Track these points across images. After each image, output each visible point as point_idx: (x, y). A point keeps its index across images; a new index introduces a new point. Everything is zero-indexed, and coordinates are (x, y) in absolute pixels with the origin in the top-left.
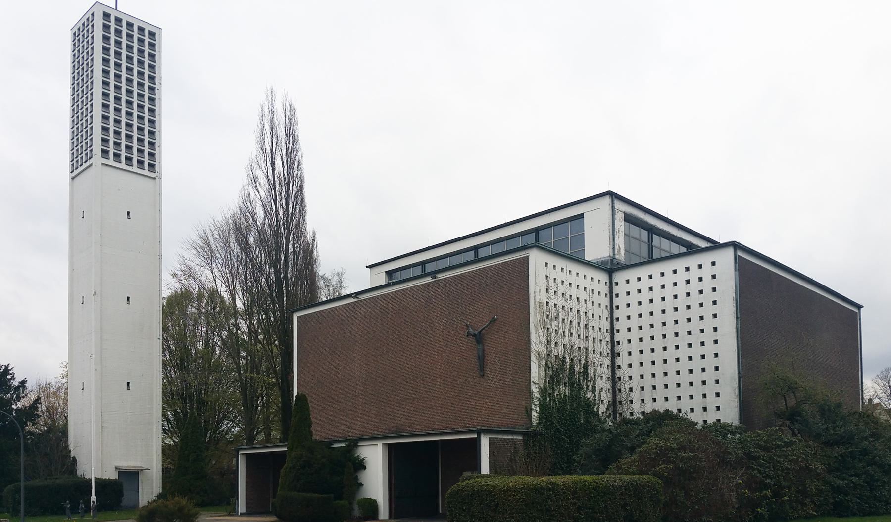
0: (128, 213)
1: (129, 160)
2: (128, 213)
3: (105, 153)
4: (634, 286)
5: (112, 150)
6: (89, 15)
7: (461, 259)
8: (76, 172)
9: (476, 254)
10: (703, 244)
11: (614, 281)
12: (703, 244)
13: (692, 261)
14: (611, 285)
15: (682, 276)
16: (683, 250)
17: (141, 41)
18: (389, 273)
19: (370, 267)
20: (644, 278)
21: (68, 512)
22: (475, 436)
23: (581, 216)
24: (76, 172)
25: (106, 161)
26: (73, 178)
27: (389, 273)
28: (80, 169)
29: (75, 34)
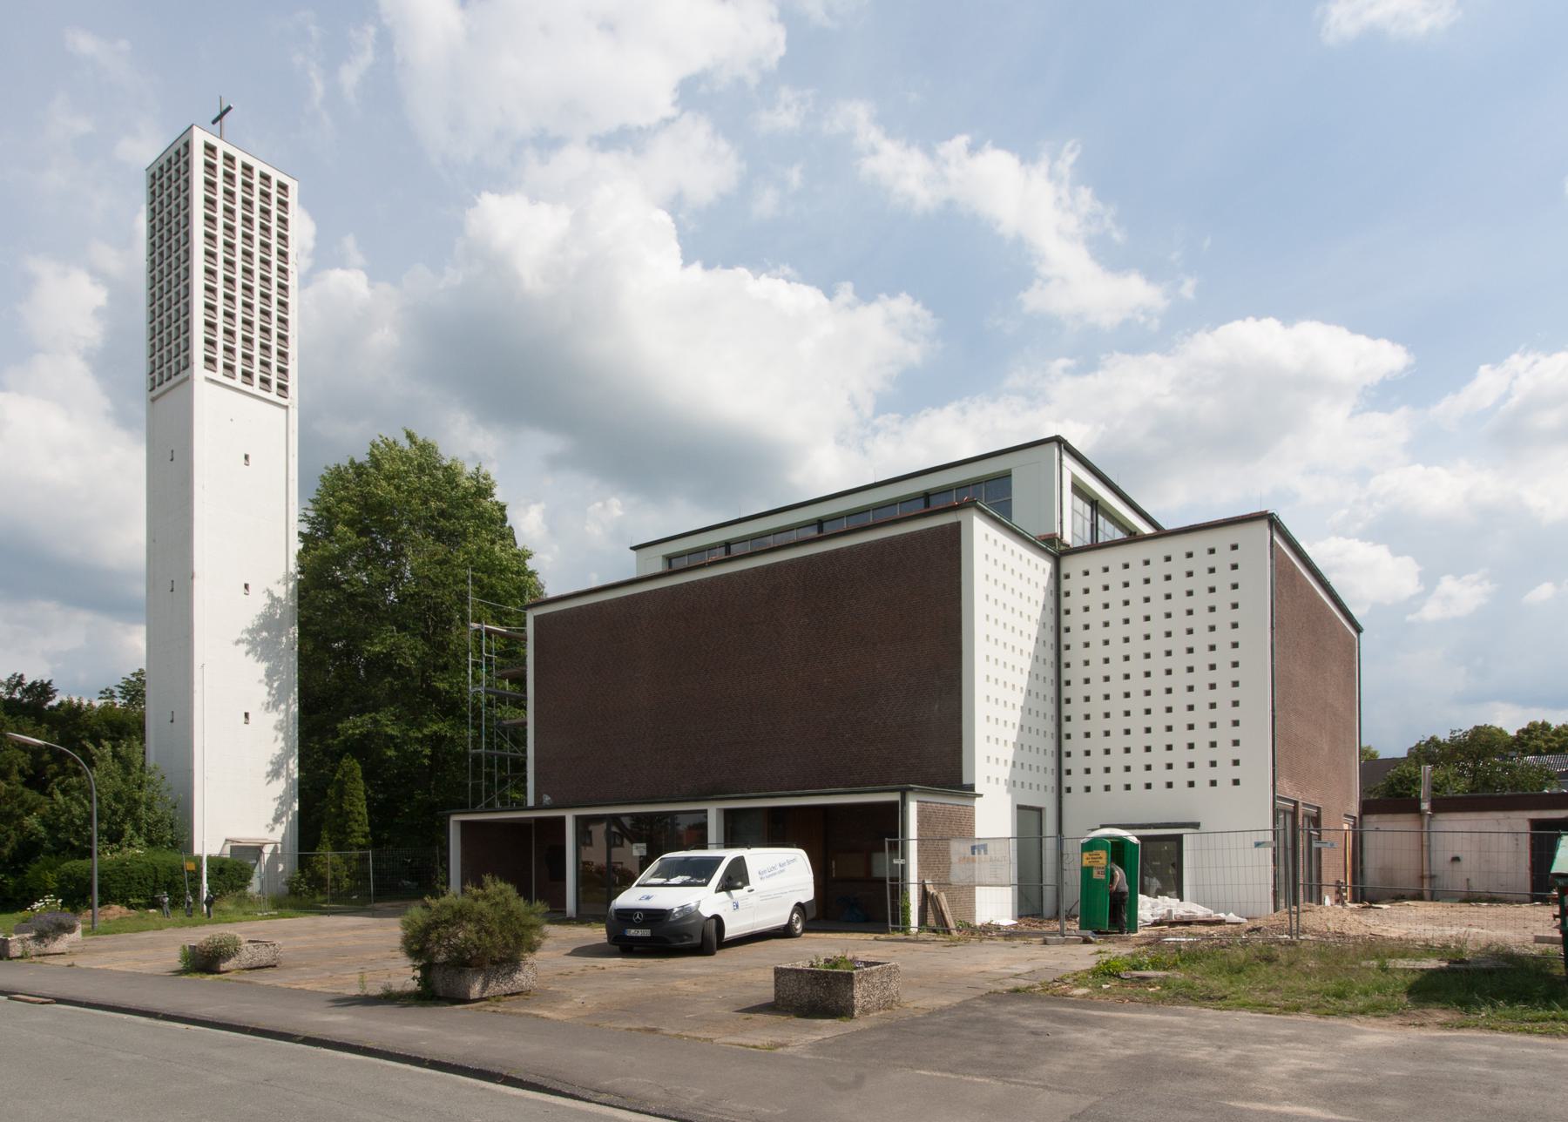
0: (246, 457)
1: (247, 375)
2: (246, 457)
3: (210, 361)
4: (1095, 582)
5: (220, 355)
6: (180, 145)
7: (794, 536)
8: (159, 390)
9: (728, 551)
10: (1147, 530)
11: (1064, 571)
12: (1147, 530)
13: (1134, 553)
14: (1058, 576)
15: (1116, 577)
16: (1119, 535)
17: (265, 195)
18: (669, 559)
19: (634, 548)
20: (1096, 571)
21: (166, 908)
22: (895, 797)
23: (1006, 476)
24: (155, 393)
25: (210, 374)
26: (153, 400)
27: (669, 559)
28: (166, 385)
29: (153, 176)
